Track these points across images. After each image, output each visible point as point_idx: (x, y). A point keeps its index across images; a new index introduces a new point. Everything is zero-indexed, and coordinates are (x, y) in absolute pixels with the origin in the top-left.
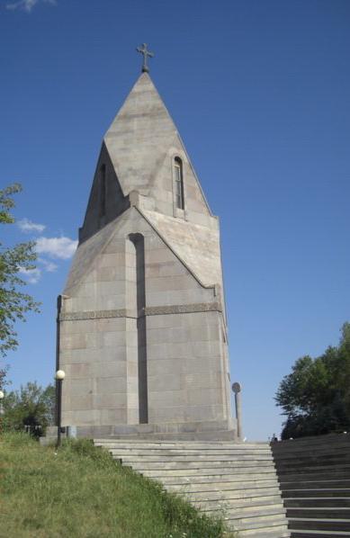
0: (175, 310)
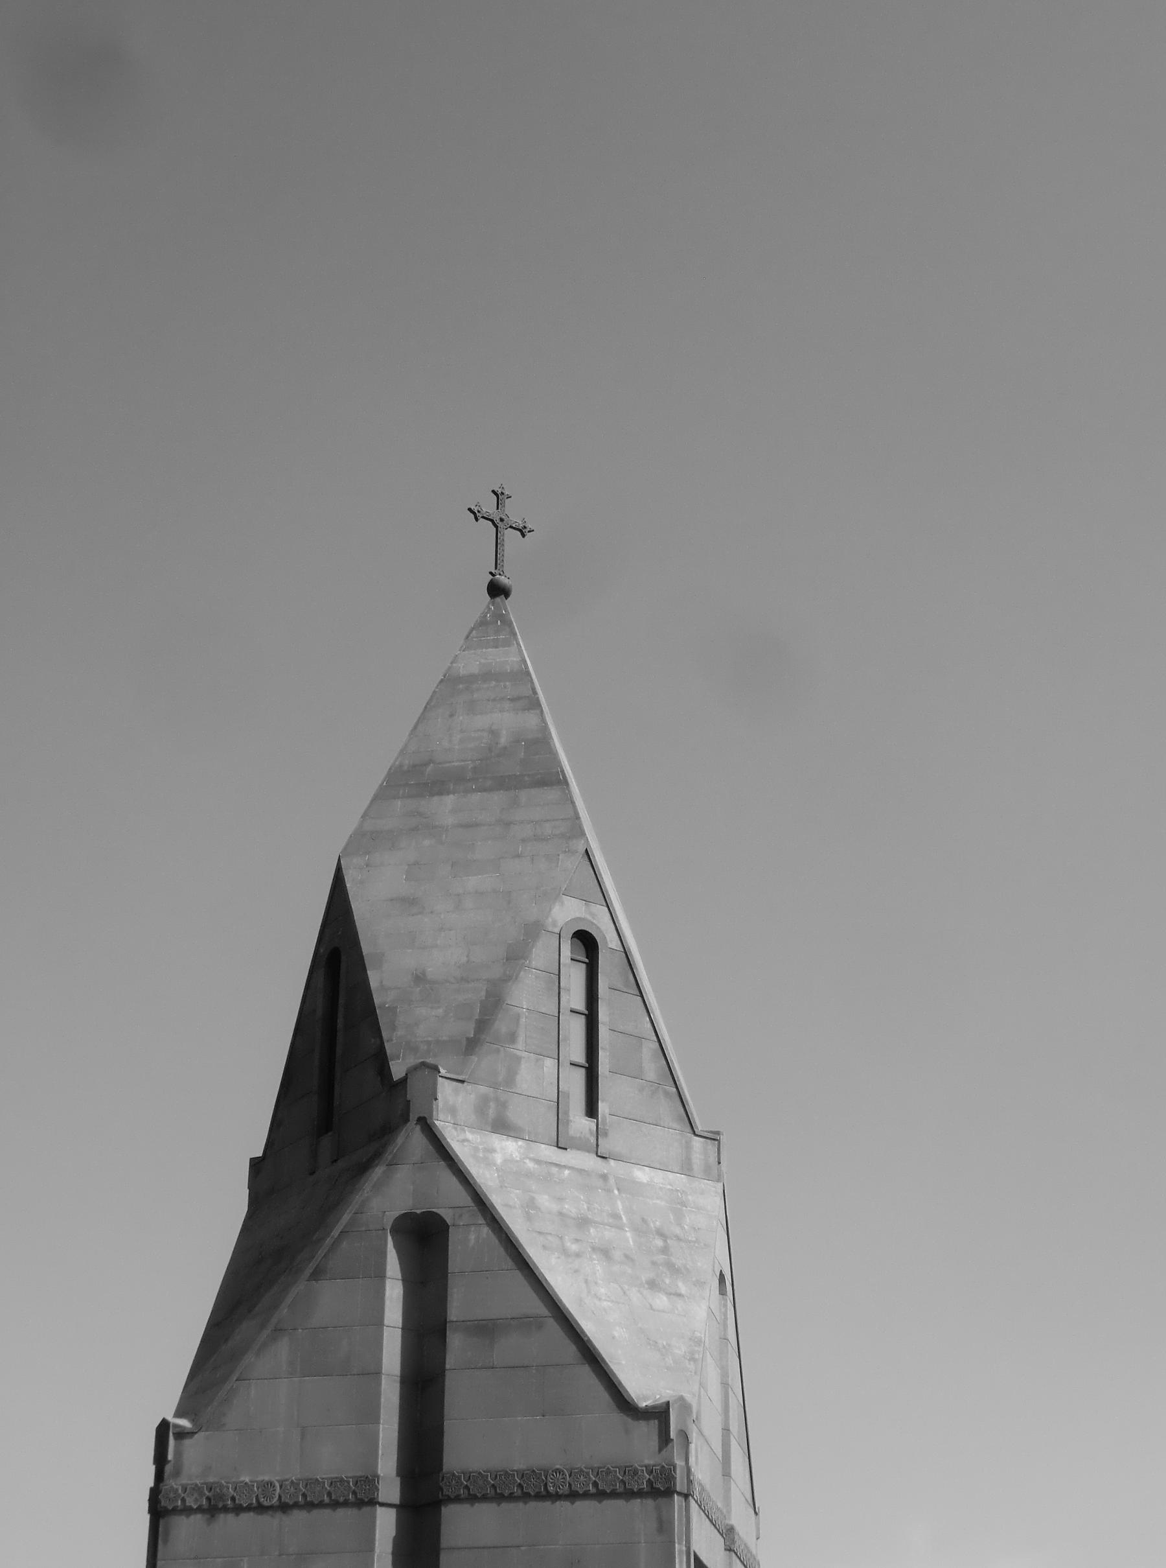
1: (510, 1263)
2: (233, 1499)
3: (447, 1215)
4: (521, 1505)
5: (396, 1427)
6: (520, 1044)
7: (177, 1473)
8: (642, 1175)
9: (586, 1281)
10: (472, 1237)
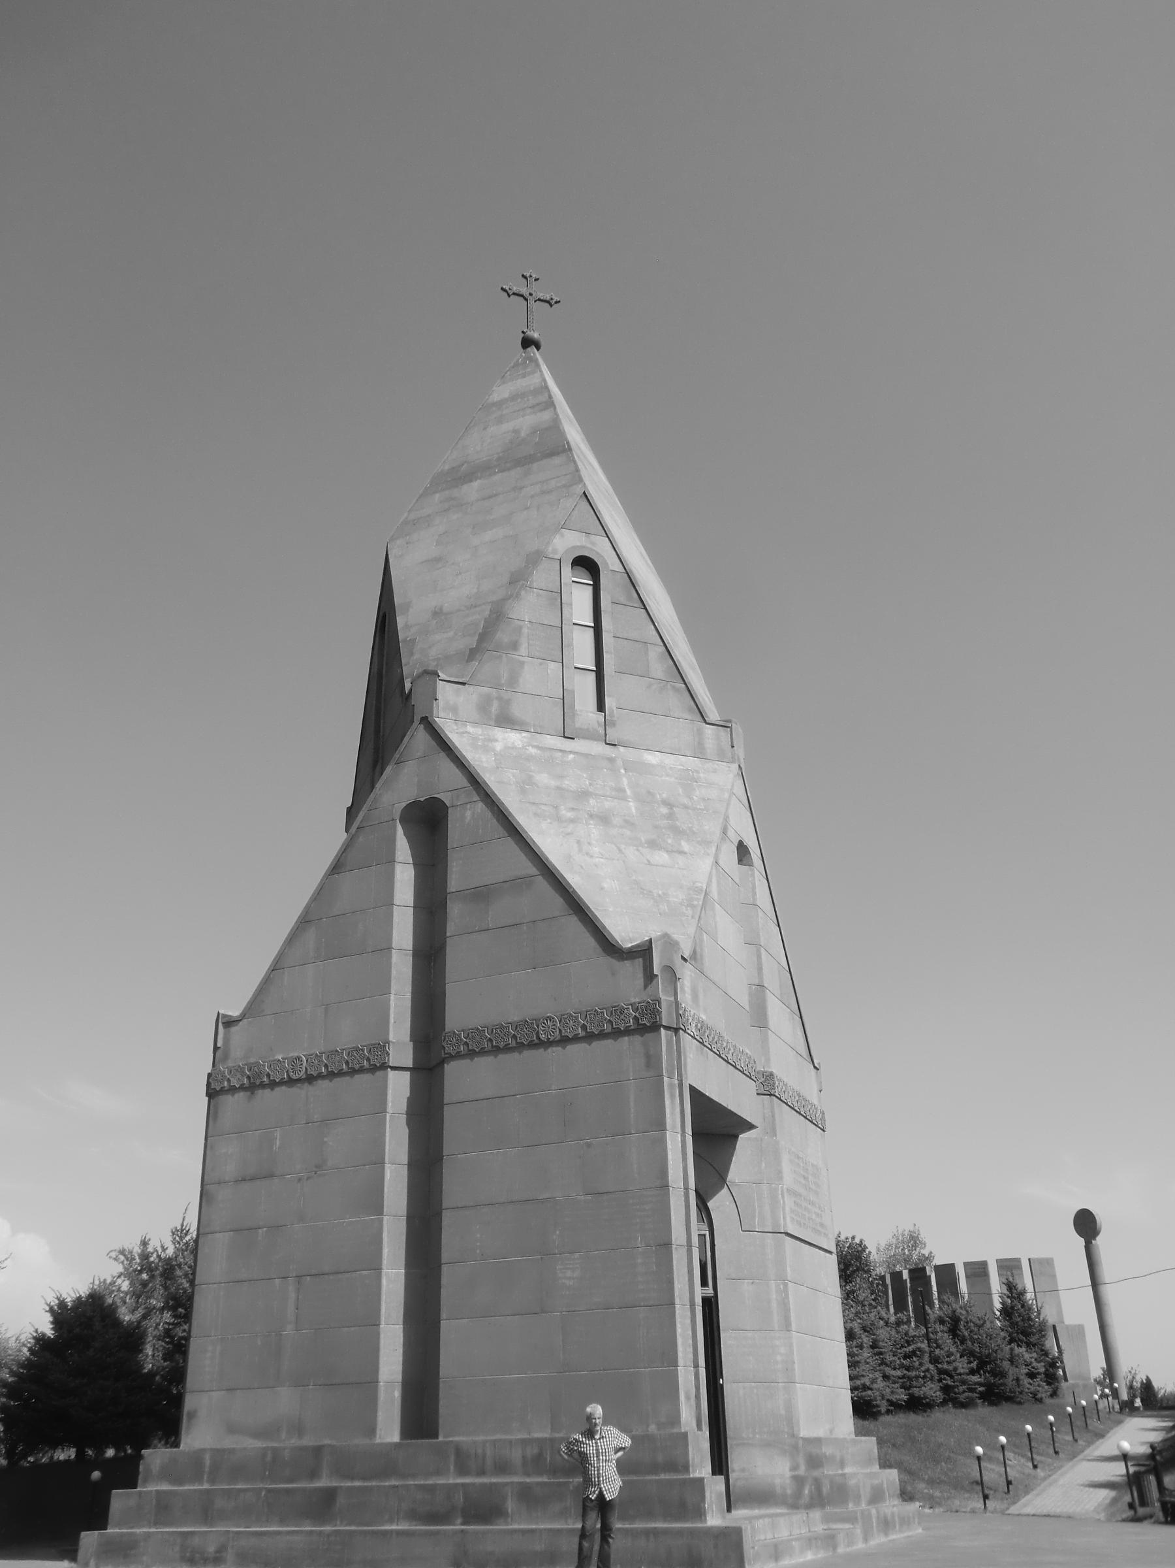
0: (527, 1038)
1: (501, 831)
2: (268, 1075)
3: (446, 798)
4: (516, 1055)
5: (409, 996)
6: (523, 650)
7: (226, 1057)
8: (652, 758)
9: (578, 842)
10: (468, 814)
